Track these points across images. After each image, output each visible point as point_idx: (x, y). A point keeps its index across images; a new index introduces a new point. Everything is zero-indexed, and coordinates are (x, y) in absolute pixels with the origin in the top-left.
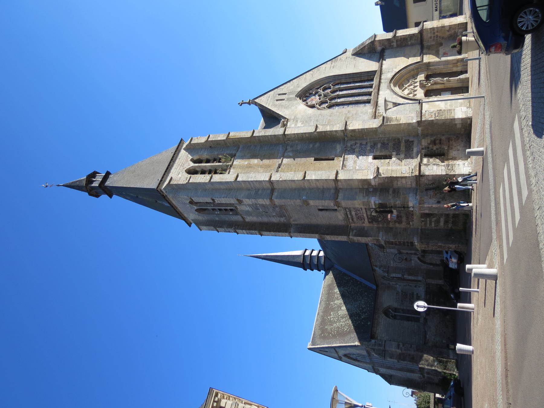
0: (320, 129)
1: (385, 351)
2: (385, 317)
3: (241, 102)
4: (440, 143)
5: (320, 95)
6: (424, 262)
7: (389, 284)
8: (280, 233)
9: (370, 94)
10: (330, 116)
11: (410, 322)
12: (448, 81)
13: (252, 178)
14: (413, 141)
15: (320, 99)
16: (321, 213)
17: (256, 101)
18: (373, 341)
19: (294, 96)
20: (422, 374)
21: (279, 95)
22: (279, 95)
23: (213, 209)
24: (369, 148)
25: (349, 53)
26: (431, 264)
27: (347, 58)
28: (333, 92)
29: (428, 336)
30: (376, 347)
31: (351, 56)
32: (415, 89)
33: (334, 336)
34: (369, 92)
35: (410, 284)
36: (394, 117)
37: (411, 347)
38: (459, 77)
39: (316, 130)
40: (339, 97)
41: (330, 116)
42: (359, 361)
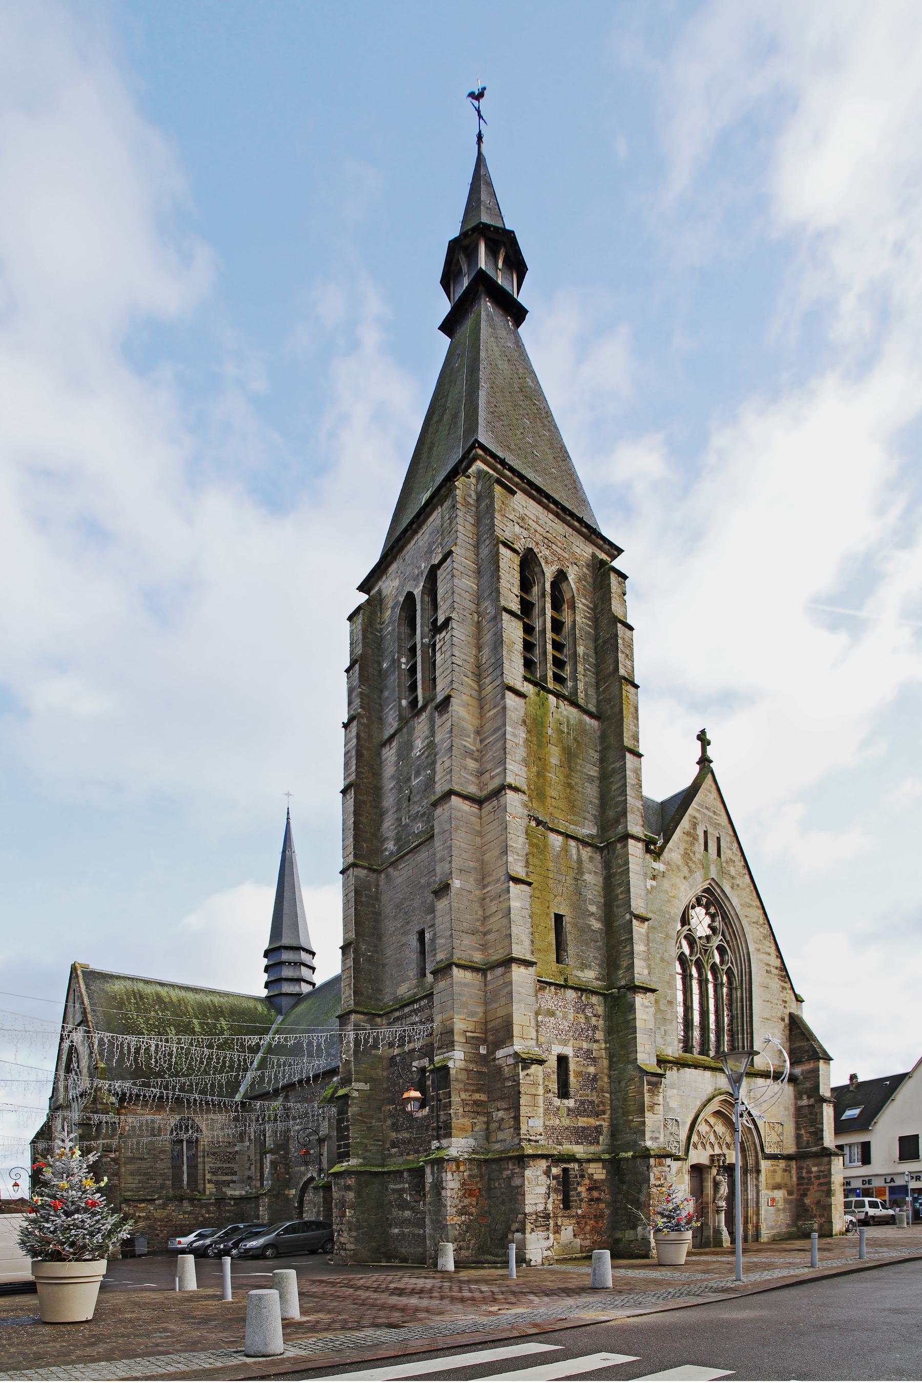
0: (639, 929)
3: (708, 737)
4: (591, 1200)
5: (708, 938)
6: (303, 1190)
8: (351, 840)
9: (704, 1051)
10: (662, 960)
12: (718, 1212)
13: (514, 735)
14: (598, 1143)
15: (700, 938)
16: (413, 940)
17: (709, 780)
19: (713, 874)
21: (718, 839)
22: (718, 839)
23: (413, 650)
24: (585, 1045)
25: (793, 1008)
27: (785, 1002)
28: (714, 968)
29: (143, 1205)
31: (787, 1011)
32: (708, 1147)
34: (709, 1050)
35: (253, 1167)
36: (660, 1099)
38: (725, 1229)
39: (638, 917)
40: (703, 982)
41: (662, 960)
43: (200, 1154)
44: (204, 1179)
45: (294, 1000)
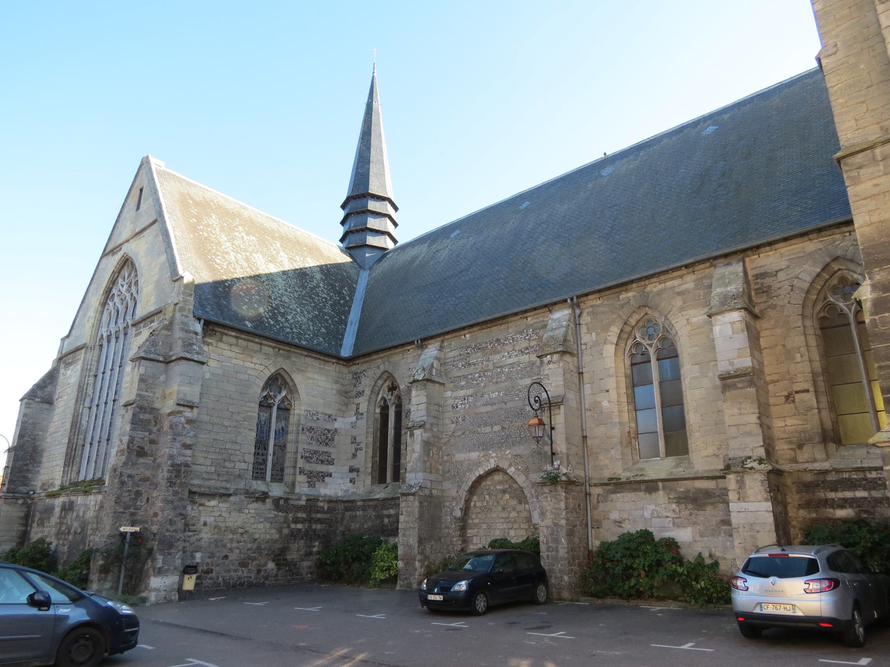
1: (167, 362)
2: (268, 374)
7: (360, 394)
11: (253, 449)
18: (198, 327)
20: (63, 488)
26: (466, 510)
29: (213, 503)
30: (178, 334)
33: (194, 229)
37: (188, 447)
42: (104, 304)
43: (291, 428)
44: (295, 467)
45: (379, 254)
